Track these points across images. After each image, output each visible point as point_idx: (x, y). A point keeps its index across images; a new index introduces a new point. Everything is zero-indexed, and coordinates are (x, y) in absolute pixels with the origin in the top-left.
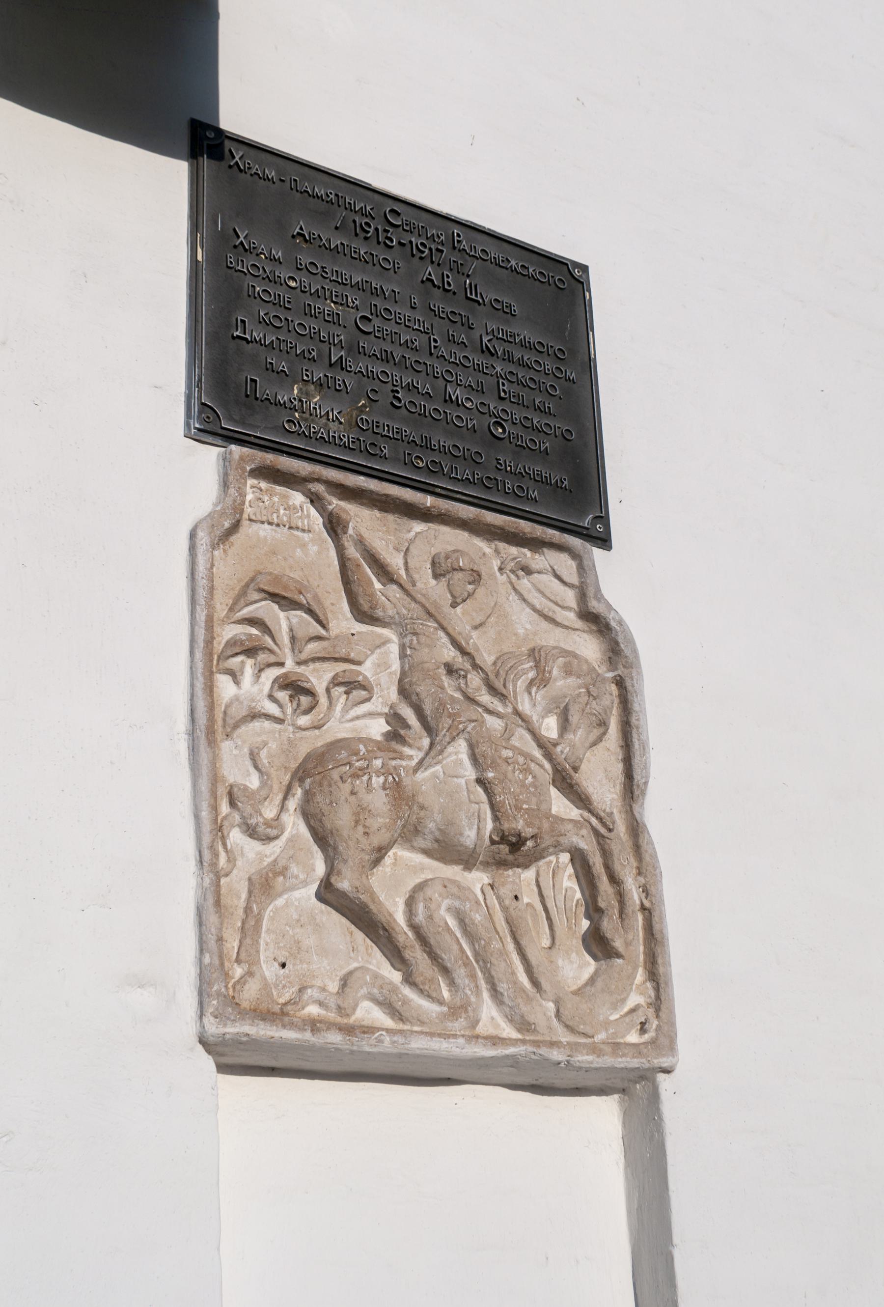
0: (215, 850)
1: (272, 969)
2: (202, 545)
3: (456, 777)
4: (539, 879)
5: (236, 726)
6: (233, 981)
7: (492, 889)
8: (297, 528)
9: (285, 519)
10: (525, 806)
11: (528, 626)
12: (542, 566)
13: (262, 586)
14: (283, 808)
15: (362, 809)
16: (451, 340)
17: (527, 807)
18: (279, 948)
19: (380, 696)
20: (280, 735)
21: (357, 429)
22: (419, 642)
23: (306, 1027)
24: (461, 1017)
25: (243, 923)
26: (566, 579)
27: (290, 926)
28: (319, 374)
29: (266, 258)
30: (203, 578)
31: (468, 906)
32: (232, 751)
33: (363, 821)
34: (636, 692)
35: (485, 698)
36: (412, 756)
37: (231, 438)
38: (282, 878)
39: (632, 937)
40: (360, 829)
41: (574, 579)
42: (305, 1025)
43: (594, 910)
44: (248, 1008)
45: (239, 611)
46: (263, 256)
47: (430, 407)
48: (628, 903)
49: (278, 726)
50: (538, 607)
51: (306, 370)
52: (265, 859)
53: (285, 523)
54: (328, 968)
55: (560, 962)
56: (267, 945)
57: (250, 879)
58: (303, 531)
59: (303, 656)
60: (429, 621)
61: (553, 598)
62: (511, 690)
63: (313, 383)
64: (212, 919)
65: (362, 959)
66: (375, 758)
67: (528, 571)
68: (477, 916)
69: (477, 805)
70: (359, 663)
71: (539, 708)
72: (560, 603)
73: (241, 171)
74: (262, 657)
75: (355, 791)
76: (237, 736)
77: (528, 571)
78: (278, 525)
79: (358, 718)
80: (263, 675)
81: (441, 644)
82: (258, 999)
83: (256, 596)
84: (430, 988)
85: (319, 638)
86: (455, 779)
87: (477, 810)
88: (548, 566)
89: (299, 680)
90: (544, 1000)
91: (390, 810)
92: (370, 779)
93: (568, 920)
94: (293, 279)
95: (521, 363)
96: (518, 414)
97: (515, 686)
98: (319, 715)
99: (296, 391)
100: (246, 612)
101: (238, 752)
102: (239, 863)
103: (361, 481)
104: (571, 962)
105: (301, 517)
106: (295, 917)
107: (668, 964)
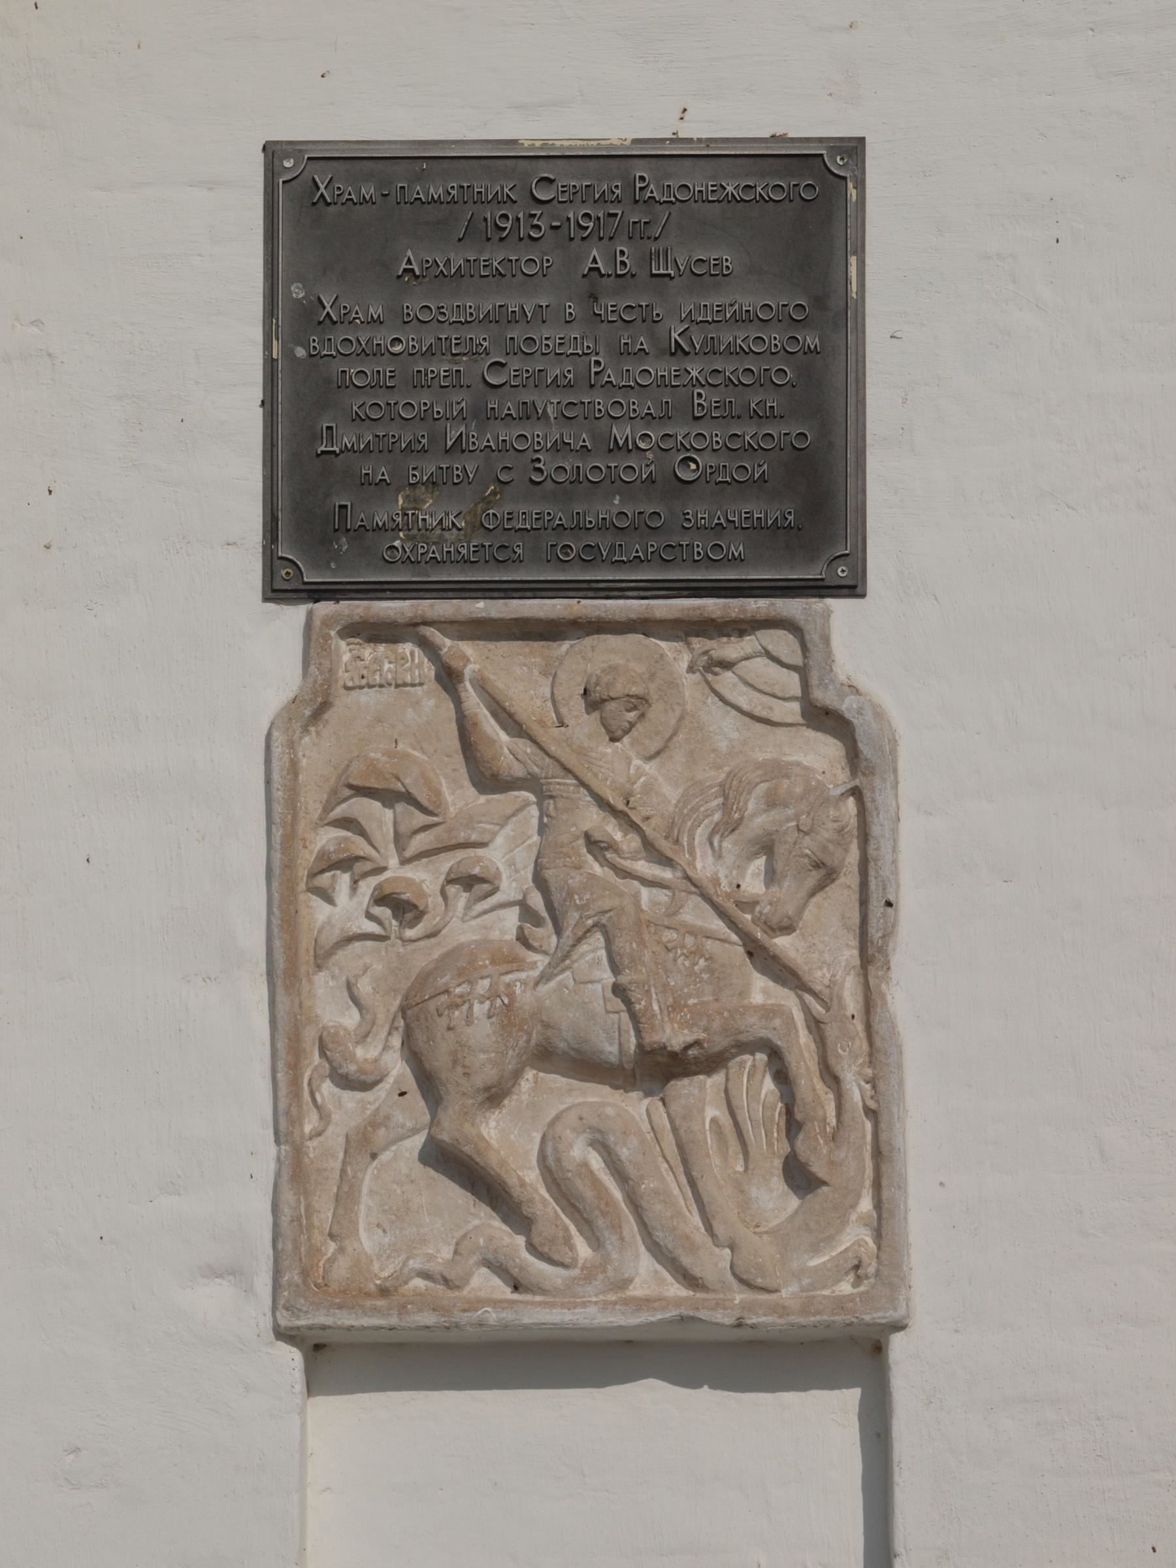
0: (291, 1116)
1: (376, 1237)
2: (278, 747)
3: (590, 982)
4: (730, 1086)
5: (330, 953)
6: (326, 1257)
7: (664, 1104)
8: (405, 685)
9: (390, 676)
10: (691, 1001)
11: (735, 735)
12: (750, 650)
13: (352, 781)
14: (386, 1048)
15: (460, 1046)
16: (624, 352)
17: (696, 1001)
18: (384, 1211)
19: (514, 880)
20: (386, 952)
21: (482, 530)
22: (556, 808)
23: (392, 1312)
24: (595, 1279)
25: (339, 1188)
26: (784, 659)
27: (397, 1184)
28: (430, 468)
29: (362, 322)
30: (278, 789)
31: (613, 1139)
32: (328, 982)
33: (461, 1061)
34: (877, 809)
35: (643, 867)
36: (535, 963)
37: (316, 593)
38: (383, 1129)
39: (844, 1154)
40: (460, 1070)
41: (798, 660)
42: (391, 1309)
43: (793, 1125)
44: (337, 1289)
45: (332, 810)
46: (358, 321)
47: (586, 465)
48: (847, 1106)
49: (383, 944)
50: (745, 706)
51: (414, 469)
52: (369, 1106)
53: (390, 682)
54: (443, 1229)
55: (754, 1192)
56: (369, 1210)
57: (347, 1136)
58: (413, 685)
59: (408, 853)
60: (568, 778)
61: (768, 689)
62: (685, 844)
63: (423, 484)
64: (288, 1196)
65: (485, 1214)
66: (482, 978)
67: (727, 665)
68: (625, 1150)
69: (617, 1015)
70: (483, 845)
71: (729, 859)
72: (779, 694)
73: (328, 204)
74: (360, 867)
75: (452, 1025)
76: (333, 964)
77: (727, 665)
78: (381, 686)
79: (485, 912)
80: (362, 884)
81: (585, 803)
82: (348, 1278)
83: (348, 792)
84: (550, 1249)
85: (426, 828)
86: (590, 986)
87: (616, 1021)
88: (760, 647)
89: (394, 893)
90: (717, 1246)
91: (497, 1042)
92: (471, 1008)
93: (766, 1135)
94: (398, 340)
95: (733, 352)
96: (717, 434)
97: (692, 838)
98: (434, 919)
99: (401, 501)
100: (339, 811)
101: (335, 982)
102: (336, 1117)
103: (480, 607)
104: (771, 1190)
105: (410, 669)
106: (405, 1171)
107: (902, 1187)
